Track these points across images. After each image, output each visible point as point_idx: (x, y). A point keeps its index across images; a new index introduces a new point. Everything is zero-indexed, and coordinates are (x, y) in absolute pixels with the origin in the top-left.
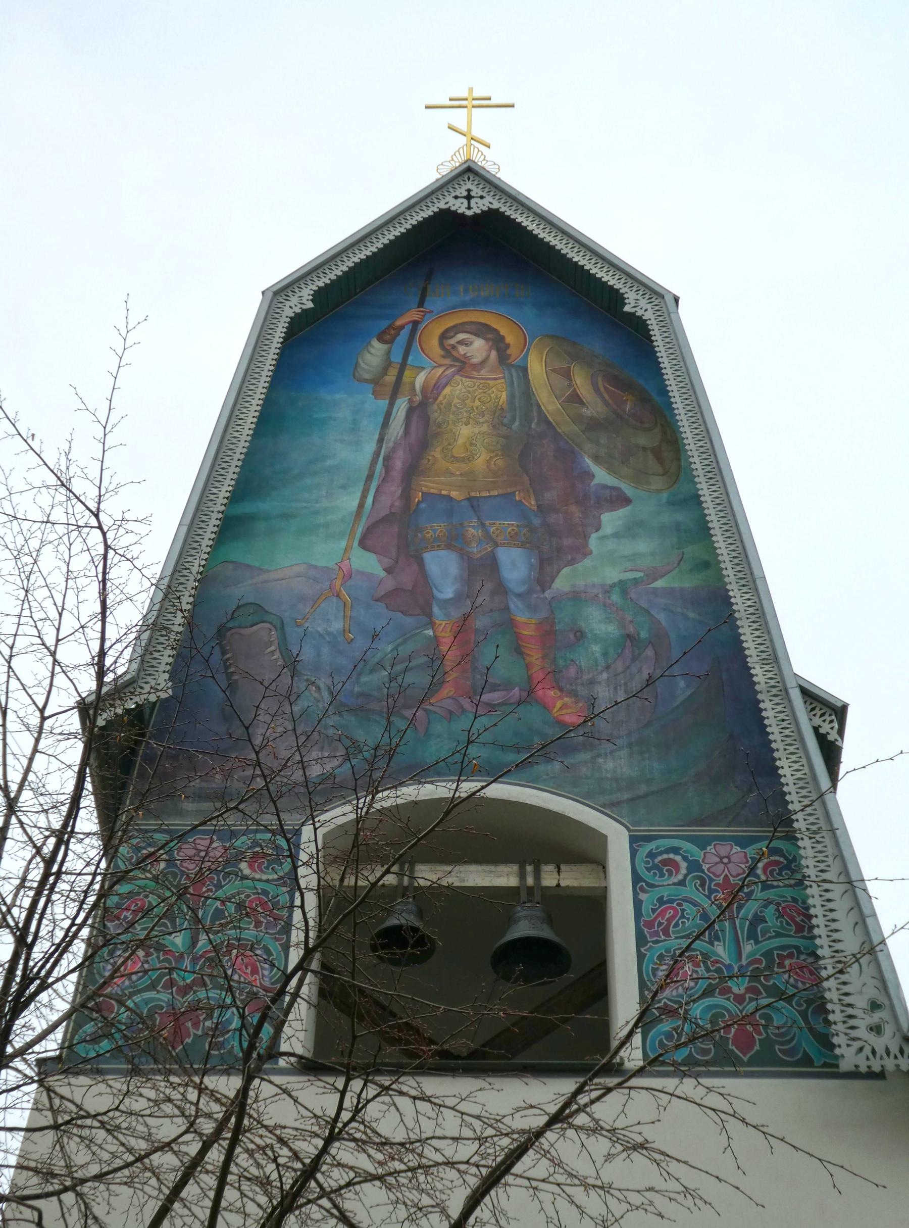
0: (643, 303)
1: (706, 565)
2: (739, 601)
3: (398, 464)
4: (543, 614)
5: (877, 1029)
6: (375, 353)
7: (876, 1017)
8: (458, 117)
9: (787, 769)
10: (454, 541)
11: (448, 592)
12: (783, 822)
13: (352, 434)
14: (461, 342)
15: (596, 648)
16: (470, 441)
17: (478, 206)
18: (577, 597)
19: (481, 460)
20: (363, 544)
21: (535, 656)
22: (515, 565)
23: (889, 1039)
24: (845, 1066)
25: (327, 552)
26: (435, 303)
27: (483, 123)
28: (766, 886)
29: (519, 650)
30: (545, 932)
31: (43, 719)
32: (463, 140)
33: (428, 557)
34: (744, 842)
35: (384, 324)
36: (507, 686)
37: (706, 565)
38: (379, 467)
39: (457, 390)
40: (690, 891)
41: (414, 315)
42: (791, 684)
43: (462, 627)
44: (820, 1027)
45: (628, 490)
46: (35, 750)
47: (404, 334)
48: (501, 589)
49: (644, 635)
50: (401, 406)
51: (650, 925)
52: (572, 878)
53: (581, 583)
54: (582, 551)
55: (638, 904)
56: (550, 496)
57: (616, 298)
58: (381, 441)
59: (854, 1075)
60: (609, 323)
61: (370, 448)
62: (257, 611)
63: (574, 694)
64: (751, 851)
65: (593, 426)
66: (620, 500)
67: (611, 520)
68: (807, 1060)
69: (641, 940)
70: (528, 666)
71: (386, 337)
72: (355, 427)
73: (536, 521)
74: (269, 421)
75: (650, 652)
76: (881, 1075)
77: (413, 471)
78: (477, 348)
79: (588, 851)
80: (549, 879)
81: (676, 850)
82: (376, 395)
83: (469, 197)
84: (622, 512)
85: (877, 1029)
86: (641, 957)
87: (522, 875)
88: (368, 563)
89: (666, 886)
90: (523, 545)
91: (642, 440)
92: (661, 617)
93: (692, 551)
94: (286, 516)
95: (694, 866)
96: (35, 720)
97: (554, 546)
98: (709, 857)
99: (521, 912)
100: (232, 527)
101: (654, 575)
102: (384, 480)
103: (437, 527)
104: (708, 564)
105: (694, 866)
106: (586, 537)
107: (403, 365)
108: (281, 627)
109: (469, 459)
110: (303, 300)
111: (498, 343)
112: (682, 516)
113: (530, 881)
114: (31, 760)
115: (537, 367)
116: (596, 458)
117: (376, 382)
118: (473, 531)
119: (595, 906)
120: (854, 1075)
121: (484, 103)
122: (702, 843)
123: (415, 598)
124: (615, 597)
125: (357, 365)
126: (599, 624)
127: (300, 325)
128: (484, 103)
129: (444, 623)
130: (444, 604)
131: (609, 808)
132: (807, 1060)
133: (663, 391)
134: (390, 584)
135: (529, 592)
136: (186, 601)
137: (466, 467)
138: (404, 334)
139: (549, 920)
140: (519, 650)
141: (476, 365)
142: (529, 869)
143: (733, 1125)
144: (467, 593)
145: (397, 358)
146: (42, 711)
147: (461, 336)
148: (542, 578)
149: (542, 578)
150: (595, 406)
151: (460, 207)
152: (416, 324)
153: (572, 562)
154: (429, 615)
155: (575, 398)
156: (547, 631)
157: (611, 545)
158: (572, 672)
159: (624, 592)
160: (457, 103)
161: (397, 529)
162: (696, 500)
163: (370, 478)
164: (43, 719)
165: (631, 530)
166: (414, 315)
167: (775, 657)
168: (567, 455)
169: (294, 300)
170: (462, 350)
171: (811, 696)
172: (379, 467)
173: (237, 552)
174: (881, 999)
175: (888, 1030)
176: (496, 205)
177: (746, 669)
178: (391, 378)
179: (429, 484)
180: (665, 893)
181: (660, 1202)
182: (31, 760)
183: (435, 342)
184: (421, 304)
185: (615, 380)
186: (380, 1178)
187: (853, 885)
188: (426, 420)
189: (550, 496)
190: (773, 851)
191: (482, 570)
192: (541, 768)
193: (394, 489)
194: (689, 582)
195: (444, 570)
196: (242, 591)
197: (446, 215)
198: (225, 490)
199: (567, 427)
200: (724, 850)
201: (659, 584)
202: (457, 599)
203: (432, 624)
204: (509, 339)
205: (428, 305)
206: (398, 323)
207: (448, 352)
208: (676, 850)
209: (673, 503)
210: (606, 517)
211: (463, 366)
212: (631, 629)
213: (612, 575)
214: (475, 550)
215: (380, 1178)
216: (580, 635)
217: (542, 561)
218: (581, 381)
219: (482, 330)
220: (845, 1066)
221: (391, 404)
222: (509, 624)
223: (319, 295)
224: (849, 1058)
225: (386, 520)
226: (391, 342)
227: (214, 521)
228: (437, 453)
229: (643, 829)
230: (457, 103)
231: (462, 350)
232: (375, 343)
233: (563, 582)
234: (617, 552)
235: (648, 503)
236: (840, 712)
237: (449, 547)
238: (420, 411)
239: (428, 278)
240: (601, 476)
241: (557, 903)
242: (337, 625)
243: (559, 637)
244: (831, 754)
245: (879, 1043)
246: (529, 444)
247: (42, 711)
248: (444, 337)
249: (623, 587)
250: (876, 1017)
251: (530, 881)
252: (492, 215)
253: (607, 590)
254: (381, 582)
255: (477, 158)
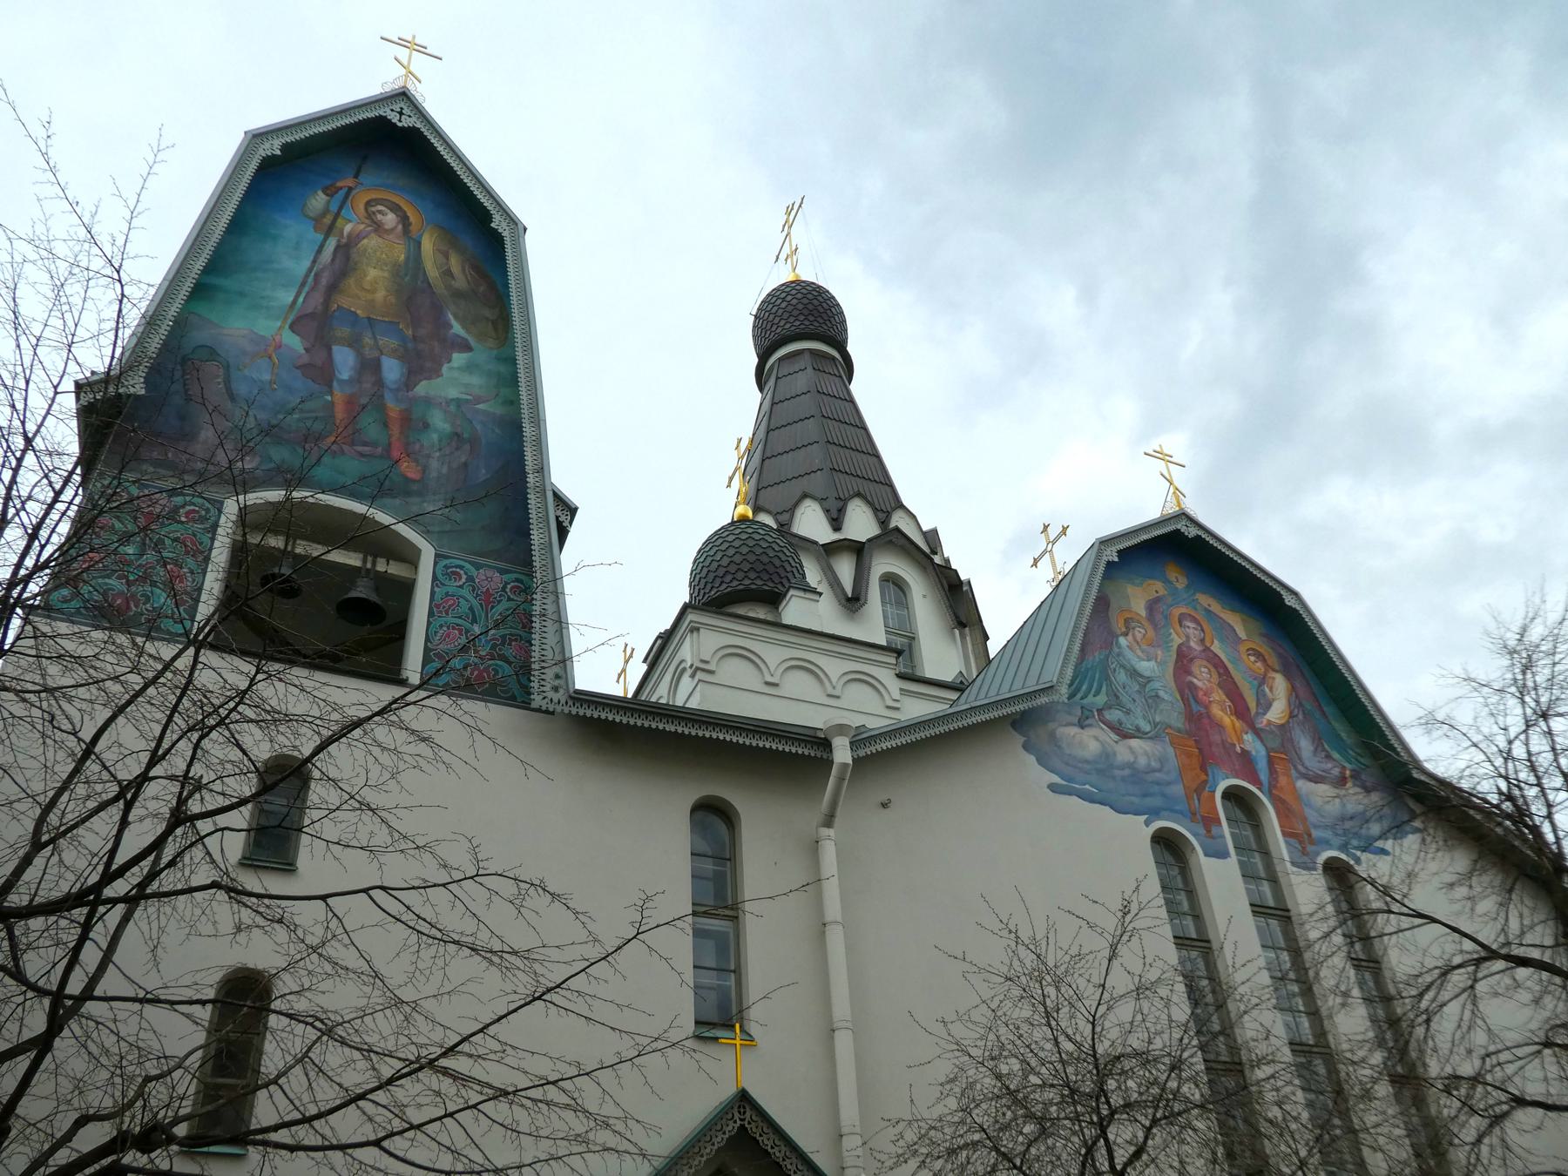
0: (504, 224)
1: (512, 403)
2: (528, 430)
3: (324, 281)
4: (403, 406)
5: (556, 689)
6: (318, 201)
7: (557, 683)
8: (403, 53)
9: (536, 536)
10: (354, 343)
11: (345, 376)
12: (528, 563)
13: (293, 252)
14: (380, 212)
15: (435, 436)
16: (374, 280)
17: (406, 122)
18: (428, 401)
19: (380, 295)
20: (291, 327)
21: (395, 431)
22: (392, 370)
23: (561, 696)
24: (534, 705)
25: (267, 327)
26: (367, 178)
27: (419, 63)
28: (509, 599)
29: (386, 425)
30: (373, 597)
31: (56, 393)
32: (403, 71)
33: (335, 348)
34: (502, 572)
35: (329, 182)
36: (374, 444)
37: (512, 403)
38: (311, 279)
39: (371, 243)
40: (465, 592)
41: (349, 182)
42: (548, 488)
43: (350, 402)
44: (524, 680)
45: (472, 341)
46: (48, 413)
47: (342, 193)
48: (380, 383)
49: (466, 436)
50: (332, 244)
51: (438, 606)
52: (395, 569)
53: (432, 393)
54: (437, 373)
55: (433, 593)
56: (422, 332)
57: (486, 216)
58: (314, 262)
59: (539, 710)
60: (478, 230)
61: (307, 264)
62: (212, 353)
63: (416, 461)
64: (506, 577)
65: (457, 294)
66: (466, 347)
67: (459, 358)
68: (513, 698)
69: (431, 614)
70: (390, 436)
71: (330, 191)
72: (297, 247)
73: (410, 345)
74: (237, 225)
75: (467, 447)
76: (553, 713)
77: (333, 288)
78: (390, 219)
79: (410, 557)
80: (381, 566)
81: (461, 567)
82: (316, 229)
83: (401, 113)
84: (465, 355)
85: (556, 689)
86: (429, 623)
87: (365, 561)
88: (294, 342)
89: (452, 586)
90: (398, 358)
91: (487, 313)
92: (479, 427)
93: (506, 392)
94: (242, 294)
95: (470, 579)
96: (51, 394)
97: (420, 365)
98: (480, 576)
99: (360, 582)
100: (200, 291)
101: (478, 400)
102: (312, 289)
103: (343, 331)
104: (514, 402)
105: (470, 579)
106: (441, 365)
107: (338, 214)
108: (227, 368)
109: (374, 291)
110: (274, 147)
111: (404, 219)
112: (503, 369)
113: (369, 566)
114: (44, 418)
115: (428, 245)
116: (456, 317)
117: (317, 221)
118: (368, 340)
119: (405, 589)
120: (539, 710)
121: (422, 49)
122: (478, 567)
123: (323, 373)
124: (452, 408)
125: (305, 205)
126: (440, 422)
127: (268, 165)
128: (422, 49)
129: (339, 395)
130: (341, 382)
131: (426, 533)
132: (513, 698)
133: (506, 286)
134: (306, 359)
135: (398, 390)
136: (164, 330)
137: (369, 297)
138: (342, 193)
139: (377, 590)
140: (386, 425)
141: (386, 232)
142: (370, 559)
143: (477, 735)
144: (356, 380)
145: (334, 208)
146: (55, 387)
147: (380, 208)
148: (409, 383)
149: (409, 383)
150: (460, 282)
151: (394, 117)
152: (350, 189)
153: (429, 378)
154: (330, 386)
155: (448, 273)
156: (406, 420)
157: (456, 374)
158: (417, 446)
159: (459, 406)
160: (403, 43)
161: (319, 322)
162: (513, 361)
163: (303, 284)
164: (56, 393)
165: (470, 368)
166: (349, 182)
167: (542, 469)
168: (437, 310)
169: (267, 145)
170: (379, 217)
171: (559, 499)
172: (311, 279)
173: (202, 309)
174: (561, 673)
175: (562, 691)
176: (418, 125)
177: (524, 474)
178: (327, 220)
179: (343, 301)
180: (451, 590)
181: (422, 763)
182: (44, 418)
183: (362, 206)
184: (356, 176)
185: (475, 268)
186: (257, 722)
187: (561, 624)
188: (348, 258)
189: (422, 332)
190: (517, 580)
191: (370, 367)
192: (388, 501)
193: (318, 299)
194: (498, 410)
195: (344, 361)
196: (200, 336)
197: (382, 121)
198: (199, 265)
199: (440, 288)
200: (490, 574)
201: (481, 406)
202: (350, 381)
203: (331, 394)
204: (412, 219)
205: (361, 179)
206: (339, 184)
207: (370, 216)
208: (461, 567)
209: (498, 359)
210: (455, 356)
211: (378, 228)
212: (459, 430)
213: (453, 393)
214: (369, 353)
215: (257, 722)
216: (426, 426)
217: (410, 372)
218: (455, 263)
219: (395, 208)
220: (534, 705)
221: (325, 240)
222: (382, 408)
223: (286, 147)
224: (537, 701)
225: (312, 316)
226: (331, 196)
227: (188, 285)
228: (351, 281)
229: (445, 551)
230: (403, 43)
231: (379, 217)
232: (320, 192)
233: (422, 388)
234: (458, 380)
235: (482, 353)
236: (572, 511)
237: (350, 346)
238: (346, 249)
239: (365, 158)
240: (457, 328)
241: (384, 582)
242: (267, 377)
243: (412, 423)
244: (563, 533)
245: (556, 697)
246: (412, 289)
247: (55, 387)
248: (368, 204)
249: (459, 402)
250: (557, 683)
251: (369, 566)
252: (414, 131)
253: (449, 402)
254: (300, 356)
255: (411, 87)
